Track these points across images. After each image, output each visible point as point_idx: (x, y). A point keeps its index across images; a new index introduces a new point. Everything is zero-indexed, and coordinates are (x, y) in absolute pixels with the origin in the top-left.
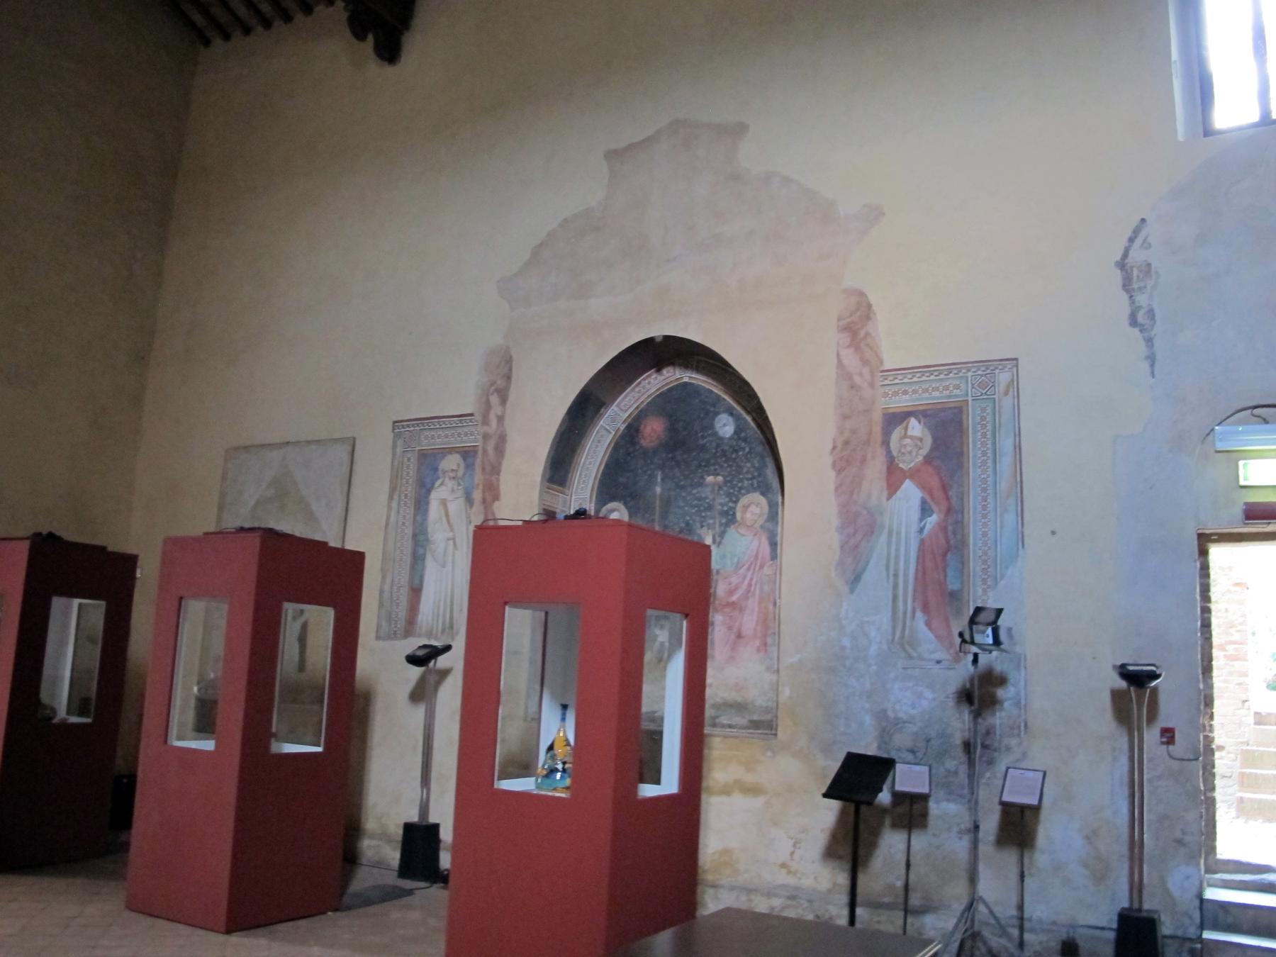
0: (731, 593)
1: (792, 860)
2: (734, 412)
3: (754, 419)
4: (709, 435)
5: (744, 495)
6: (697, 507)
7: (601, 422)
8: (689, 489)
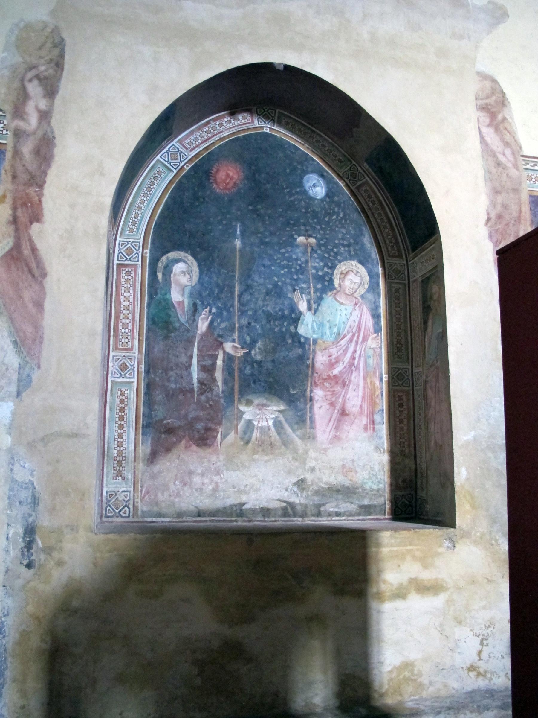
0: (332, 365)
1: (480, 659)
2: (325, 174)
3: (347, 185)
4: (297, 193)
5: (340, 262)
6: (286, 268)
7: (158, 157)
8: (276, 248)
